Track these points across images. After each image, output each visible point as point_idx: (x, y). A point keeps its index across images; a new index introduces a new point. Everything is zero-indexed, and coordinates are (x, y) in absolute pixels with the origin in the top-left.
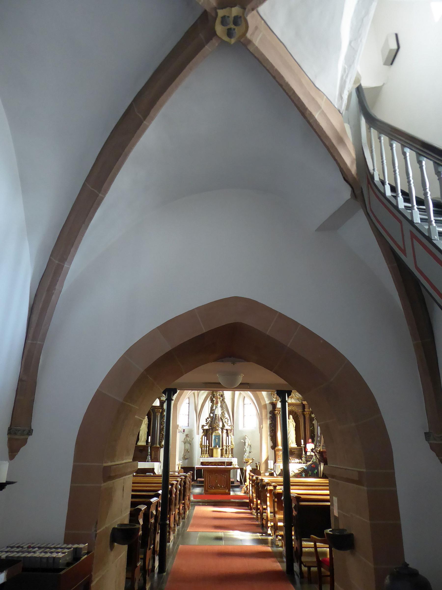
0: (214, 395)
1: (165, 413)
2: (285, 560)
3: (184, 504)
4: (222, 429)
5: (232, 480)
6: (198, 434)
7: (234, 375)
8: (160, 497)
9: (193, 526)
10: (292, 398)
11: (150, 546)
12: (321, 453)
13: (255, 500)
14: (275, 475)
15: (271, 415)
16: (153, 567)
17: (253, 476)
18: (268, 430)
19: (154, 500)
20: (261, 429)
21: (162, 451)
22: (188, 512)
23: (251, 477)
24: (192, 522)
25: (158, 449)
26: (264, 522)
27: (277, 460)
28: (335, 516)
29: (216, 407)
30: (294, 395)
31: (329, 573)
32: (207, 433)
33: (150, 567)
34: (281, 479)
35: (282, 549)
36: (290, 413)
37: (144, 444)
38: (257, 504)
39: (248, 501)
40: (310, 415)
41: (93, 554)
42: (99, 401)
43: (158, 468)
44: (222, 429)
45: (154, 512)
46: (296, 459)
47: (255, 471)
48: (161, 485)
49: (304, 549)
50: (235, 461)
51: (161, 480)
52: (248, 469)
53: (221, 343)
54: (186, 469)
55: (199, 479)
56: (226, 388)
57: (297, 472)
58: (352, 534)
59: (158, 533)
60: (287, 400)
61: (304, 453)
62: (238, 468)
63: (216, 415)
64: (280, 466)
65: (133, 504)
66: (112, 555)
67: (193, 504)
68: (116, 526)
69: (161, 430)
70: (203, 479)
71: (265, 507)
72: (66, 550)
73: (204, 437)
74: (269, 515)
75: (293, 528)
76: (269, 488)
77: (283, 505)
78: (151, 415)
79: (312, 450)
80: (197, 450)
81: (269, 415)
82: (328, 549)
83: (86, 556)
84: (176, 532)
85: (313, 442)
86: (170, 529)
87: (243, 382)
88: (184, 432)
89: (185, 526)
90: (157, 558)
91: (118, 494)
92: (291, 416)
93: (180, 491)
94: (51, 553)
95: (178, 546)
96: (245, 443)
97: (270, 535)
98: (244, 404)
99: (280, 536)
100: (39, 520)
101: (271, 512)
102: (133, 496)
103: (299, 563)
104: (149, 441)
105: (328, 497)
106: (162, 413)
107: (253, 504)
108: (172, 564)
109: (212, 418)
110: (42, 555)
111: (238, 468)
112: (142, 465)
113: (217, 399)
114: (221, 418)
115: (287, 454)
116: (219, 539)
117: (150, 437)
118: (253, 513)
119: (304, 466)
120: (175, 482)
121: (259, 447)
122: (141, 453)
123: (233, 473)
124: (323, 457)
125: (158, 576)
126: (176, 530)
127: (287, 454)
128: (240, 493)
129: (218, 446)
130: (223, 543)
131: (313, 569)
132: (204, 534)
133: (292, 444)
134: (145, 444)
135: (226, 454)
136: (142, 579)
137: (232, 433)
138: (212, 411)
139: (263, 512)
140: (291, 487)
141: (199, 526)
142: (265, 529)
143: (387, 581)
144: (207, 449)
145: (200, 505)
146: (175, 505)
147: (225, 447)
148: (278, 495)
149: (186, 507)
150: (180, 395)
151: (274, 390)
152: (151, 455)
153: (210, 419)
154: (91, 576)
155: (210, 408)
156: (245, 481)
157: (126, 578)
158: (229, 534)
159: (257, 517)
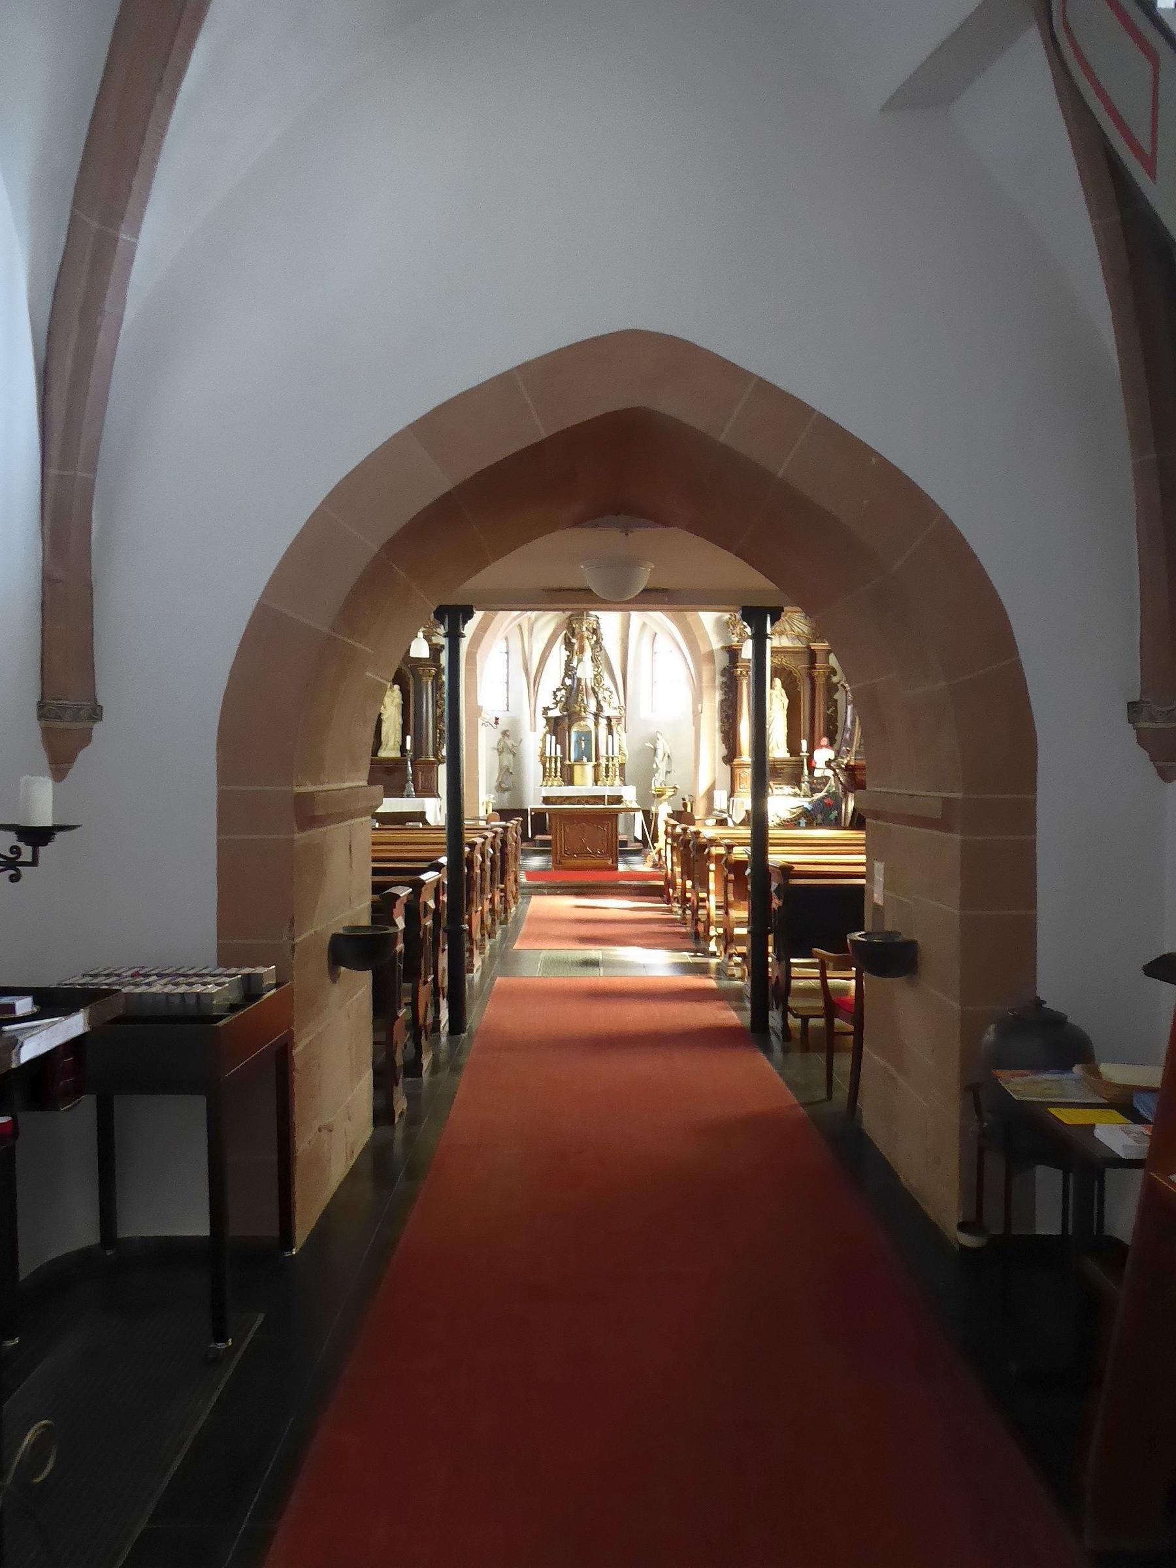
0: (574, 629)
1: (445, 678)
2: (748, 1005)
3: (502, 891)
4: (597, 716)
5: (621, 838)
6: (534, 728)
7: (626, 566)
8: (444, 870)
9: (527, 936)
10: (781, 633)
11: (426, 977)
12: (850, 770)
13: (679, 881)
14: (730, 823)
15: (724, 679)
16: (437, 1022)
17: (674, 826)
18: (716, 716)
19: (429, 876)
20: (697, 715)
21: (442, 771)
22: (513, 909)
23: (669, 829)
24: (524, 928)
25: (432, 766)
26: (701, 928)
27: (737, 789)
28: (876, 905)
29: (580, 661)
30: (787, 627)
31: (851, 1028)
32: (557, 727)
33: (430, 1021)
34: (746, 832)
35: (744, 984)
36: (776, 673)
37: (396, 754)
38: (684, 890)
39: (662, 883)
40: (828, 678)
41: (291, 987)
42: (266, 632)
43: (435, 810)
44: (597, 716)
45: (432, 904)
46: (785, 787)
47: (682, 815)
48: (445, 847)
49: (794, 983)
50: (630, 795)
51: (443, 836)
52: (663, 811)
53: (592, 470)
54: (505, 814)
55: (538, 837)
56: (606, 602)
57: (787, 816)
58: (915, 942)
59: (444, 950)
60: (769, 631)
61: (806, 772)
62: (638, 810)
63: (579, 680)
64: (744, 802)
65: (377, 888)
66: (336, 991)
67: (525, 891)
68: (341, 931)
69: (438, 719)
70: (549, 837)
71: (703, 895)
72: (226, 980)
73: (548, 736)
74: (714, 912)
75: (771, 937)
76: (715, 851)
77: (749, 887)
78: (407, 684)
79: (828, 764)
80: (532, 769)
81: (719, 680)
82: (853, 983)
83: (274, 991)
84: (487, 951)
85: (831, 744)
86: (472, 944)
87: (651, 586)
88: (496, 723)
89: (508, 938)
90: (444, 1004)
91: (337, 862)
92: (778, 682)
93: (492, 860)
94: (191, 984)
95: (493, 979)
96: (655, 750)
97: (713, 955)
98: (654, 653)
99: (739, 955)
100: (145, 901)
101: (718, 907)
102: (376, 871)
103: (781, 1009)
104: (408, 747)
105: (863, 869)
106: (437, 677)
107: (675, 889)
108: (478, 1016)
109: (569, 690)
110: (170, 989)
111: (638, 810)
112: (390, 805)
113: (581, 639)
114: (593, 689)
115: (763, 774)
116: (594, 963)
117: (409, 738)
118: (675, 909)
119: (805, 803)
120: (479, 840)
121: (693, 753)
122: (391, 777)
123: (626, 819)
124: (854, 778)
125: (448, 1040)
126: (488, 947)
127: (763, 774)
128: (641, 866)
129: (585, 759)
130: (601, 971)
131: (812, 1022)
132: (554, 954)
133: (778, 749)
134: (399, 755)
135: (607, 776)
136: (410, 1044)
137: (622, 725)
138: (569, 670)
139: (699, 907)
140: (770, 848)
141: (541, 937)
142: (702, 943)
143: (990, 1036)
144: (559, 765)
145: (544, 894)
146: (482, 892)
147: (603, 762)
148: (739, 866)
149: (510, 897)
150: (483, 628)
151: (734, 608)
152: (415, 781)
153: (563, 692)
154: (290, 1035)
155: (563, 663)
156: (655, 839)
157: (375, 1043)
158: (612, 953)
159: (684, 918)
